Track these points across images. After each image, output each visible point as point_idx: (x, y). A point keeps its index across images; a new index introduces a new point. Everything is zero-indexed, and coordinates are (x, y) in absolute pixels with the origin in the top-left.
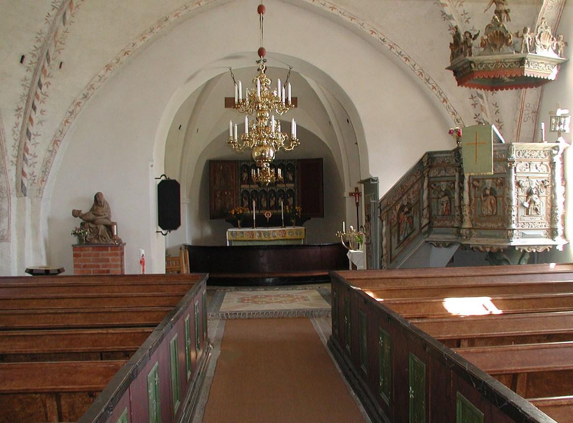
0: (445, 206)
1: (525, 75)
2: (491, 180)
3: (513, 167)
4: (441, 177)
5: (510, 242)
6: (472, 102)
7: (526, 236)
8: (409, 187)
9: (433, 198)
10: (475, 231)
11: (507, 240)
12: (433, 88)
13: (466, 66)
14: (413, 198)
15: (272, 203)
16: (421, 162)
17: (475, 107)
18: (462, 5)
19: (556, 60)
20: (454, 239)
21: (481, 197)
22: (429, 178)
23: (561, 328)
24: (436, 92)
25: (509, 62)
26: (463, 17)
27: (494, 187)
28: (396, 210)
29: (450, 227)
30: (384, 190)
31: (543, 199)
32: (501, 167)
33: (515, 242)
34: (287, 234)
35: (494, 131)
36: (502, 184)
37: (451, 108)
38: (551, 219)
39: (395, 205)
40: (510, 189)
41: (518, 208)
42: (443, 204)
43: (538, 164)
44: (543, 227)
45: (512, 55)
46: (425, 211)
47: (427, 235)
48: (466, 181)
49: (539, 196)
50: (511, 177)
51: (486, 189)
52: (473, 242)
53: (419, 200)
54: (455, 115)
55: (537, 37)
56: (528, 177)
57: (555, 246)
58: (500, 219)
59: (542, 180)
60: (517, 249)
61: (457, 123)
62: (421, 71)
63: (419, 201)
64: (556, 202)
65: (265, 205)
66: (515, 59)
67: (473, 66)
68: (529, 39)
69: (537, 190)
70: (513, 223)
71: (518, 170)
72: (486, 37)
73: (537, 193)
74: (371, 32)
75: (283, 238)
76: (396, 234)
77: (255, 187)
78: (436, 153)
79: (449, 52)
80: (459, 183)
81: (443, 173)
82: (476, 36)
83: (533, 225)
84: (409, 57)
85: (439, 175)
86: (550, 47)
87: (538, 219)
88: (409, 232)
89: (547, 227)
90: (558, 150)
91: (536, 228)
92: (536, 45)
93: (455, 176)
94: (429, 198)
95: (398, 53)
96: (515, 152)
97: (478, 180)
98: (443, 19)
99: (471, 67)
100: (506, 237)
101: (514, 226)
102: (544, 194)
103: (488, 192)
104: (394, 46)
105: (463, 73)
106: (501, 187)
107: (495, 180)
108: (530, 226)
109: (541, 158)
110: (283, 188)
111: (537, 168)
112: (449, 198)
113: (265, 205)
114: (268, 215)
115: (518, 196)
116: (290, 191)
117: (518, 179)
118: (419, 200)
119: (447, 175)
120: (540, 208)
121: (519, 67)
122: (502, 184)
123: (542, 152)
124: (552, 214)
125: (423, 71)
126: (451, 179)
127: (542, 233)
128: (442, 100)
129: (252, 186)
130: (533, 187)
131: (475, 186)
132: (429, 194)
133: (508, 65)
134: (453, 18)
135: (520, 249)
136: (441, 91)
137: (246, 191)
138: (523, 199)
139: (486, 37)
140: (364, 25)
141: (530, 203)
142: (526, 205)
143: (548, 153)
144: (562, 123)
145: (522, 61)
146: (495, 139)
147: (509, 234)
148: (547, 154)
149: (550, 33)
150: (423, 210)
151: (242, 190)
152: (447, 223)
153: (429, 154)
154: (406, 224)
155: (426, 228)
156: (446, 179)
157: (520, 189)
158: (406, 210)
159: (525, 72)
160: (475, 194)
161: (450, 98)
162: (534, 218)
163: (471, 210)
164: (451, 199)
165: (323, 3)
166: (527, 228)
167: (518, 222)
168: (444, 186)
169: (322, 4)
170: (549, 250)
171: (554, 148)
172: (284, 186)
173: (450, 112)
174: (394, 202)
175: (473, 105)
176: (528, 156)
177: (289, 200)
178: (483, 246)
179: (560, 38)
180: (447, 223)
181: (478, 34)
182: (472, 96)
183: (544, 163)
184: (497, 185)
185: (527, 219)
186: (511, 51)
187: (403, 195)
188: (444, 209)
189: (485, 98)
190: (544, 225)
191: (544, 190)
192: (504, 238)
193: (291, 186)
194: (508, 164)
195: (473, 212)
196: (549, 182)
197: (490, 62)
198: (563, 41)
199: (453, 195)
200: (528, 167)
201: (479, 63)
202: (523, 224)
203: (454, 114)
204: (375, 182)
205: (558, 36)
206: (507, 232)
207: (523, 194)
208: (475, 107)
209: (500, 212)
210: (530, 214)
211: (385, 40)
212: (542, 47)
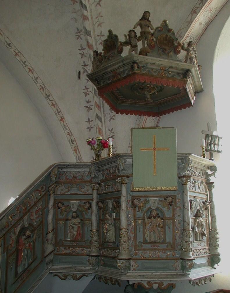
0: (76, 229)
4: (72, 195)
6: (88, 125)
8: (32, 204)
9: (61, 220)
10: (135, 263)
11: (181, 273)
14: (37, 218)
17: (90, 131)
18: (101, 26)
24: (55, 109)
25: (172, 72)
26: (98, 38)
28: (15, 233)
37: (68, 129)
39: (15, 226)
46: (50, 236)
53: (42, 222)
54: (70, 136)
61: (71, 144)
62: (43, 86)
63: (43, 223)
76: (14, 265)
80: (97, 203)
81: (74, 190)
84: (33, 69)
85: (69, 193)
88: (30, 261)
94: (56, 220)
95: (22, 62)
97: (138, 198)
104: (19, 54)
106: (171, 207)
118: (42, 222)
119: (79, 193)
125: (44, 85)
126: (89, 197)
128: (60, 118)
132: (55, 214)
134: (90, 34)
150: (47, 234)
152: (78, 250)
154: (28, 251)
155: (51, 257)
158: (28, 233)
161: (68, 119)
168: (75, 205)
173: (66, 132)
174: (13, 223)
175: (88, 128)
178: (149, 283)
182: (89, 119)
187: (25, 214)
189: (103, 122)
203: (69, 134)
208: (90, 131)
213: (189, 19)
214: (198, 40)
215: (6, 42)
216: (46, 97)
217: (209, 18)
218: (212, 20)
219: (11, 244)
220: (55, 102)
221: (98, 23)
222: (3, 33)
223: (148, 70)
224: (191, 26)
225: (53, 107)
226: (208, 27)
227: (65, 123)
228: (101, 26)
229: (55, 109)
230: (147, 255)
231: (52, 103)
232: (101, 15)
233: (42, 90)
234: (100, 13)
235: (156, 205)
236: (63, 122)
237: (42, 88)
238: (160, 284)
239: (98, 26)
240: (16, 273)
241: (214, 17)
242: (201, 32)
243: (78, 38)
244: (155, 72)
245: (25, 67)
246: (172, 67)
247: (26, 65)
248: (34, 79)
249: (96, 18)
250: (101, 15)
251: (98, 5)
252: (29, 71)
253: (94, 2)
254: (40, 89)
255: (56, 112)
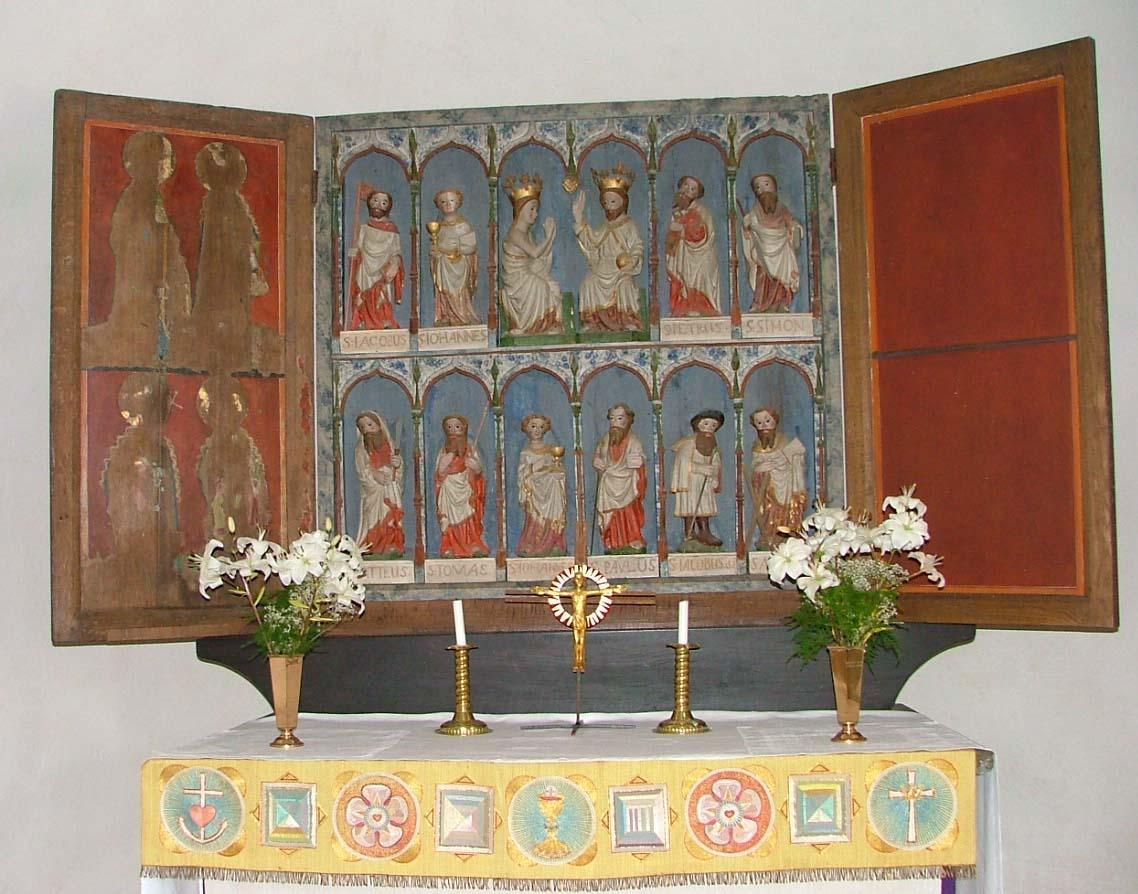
23: (319, 479)
53: (320, 822)
110: (716, 348)
114: (579, 603)
116: (776, 374)
129: (437, 340)
137: (375, 378)
151: (347, 375)
172: (718, 330)
177: (766, 460)
193: (790, 329)
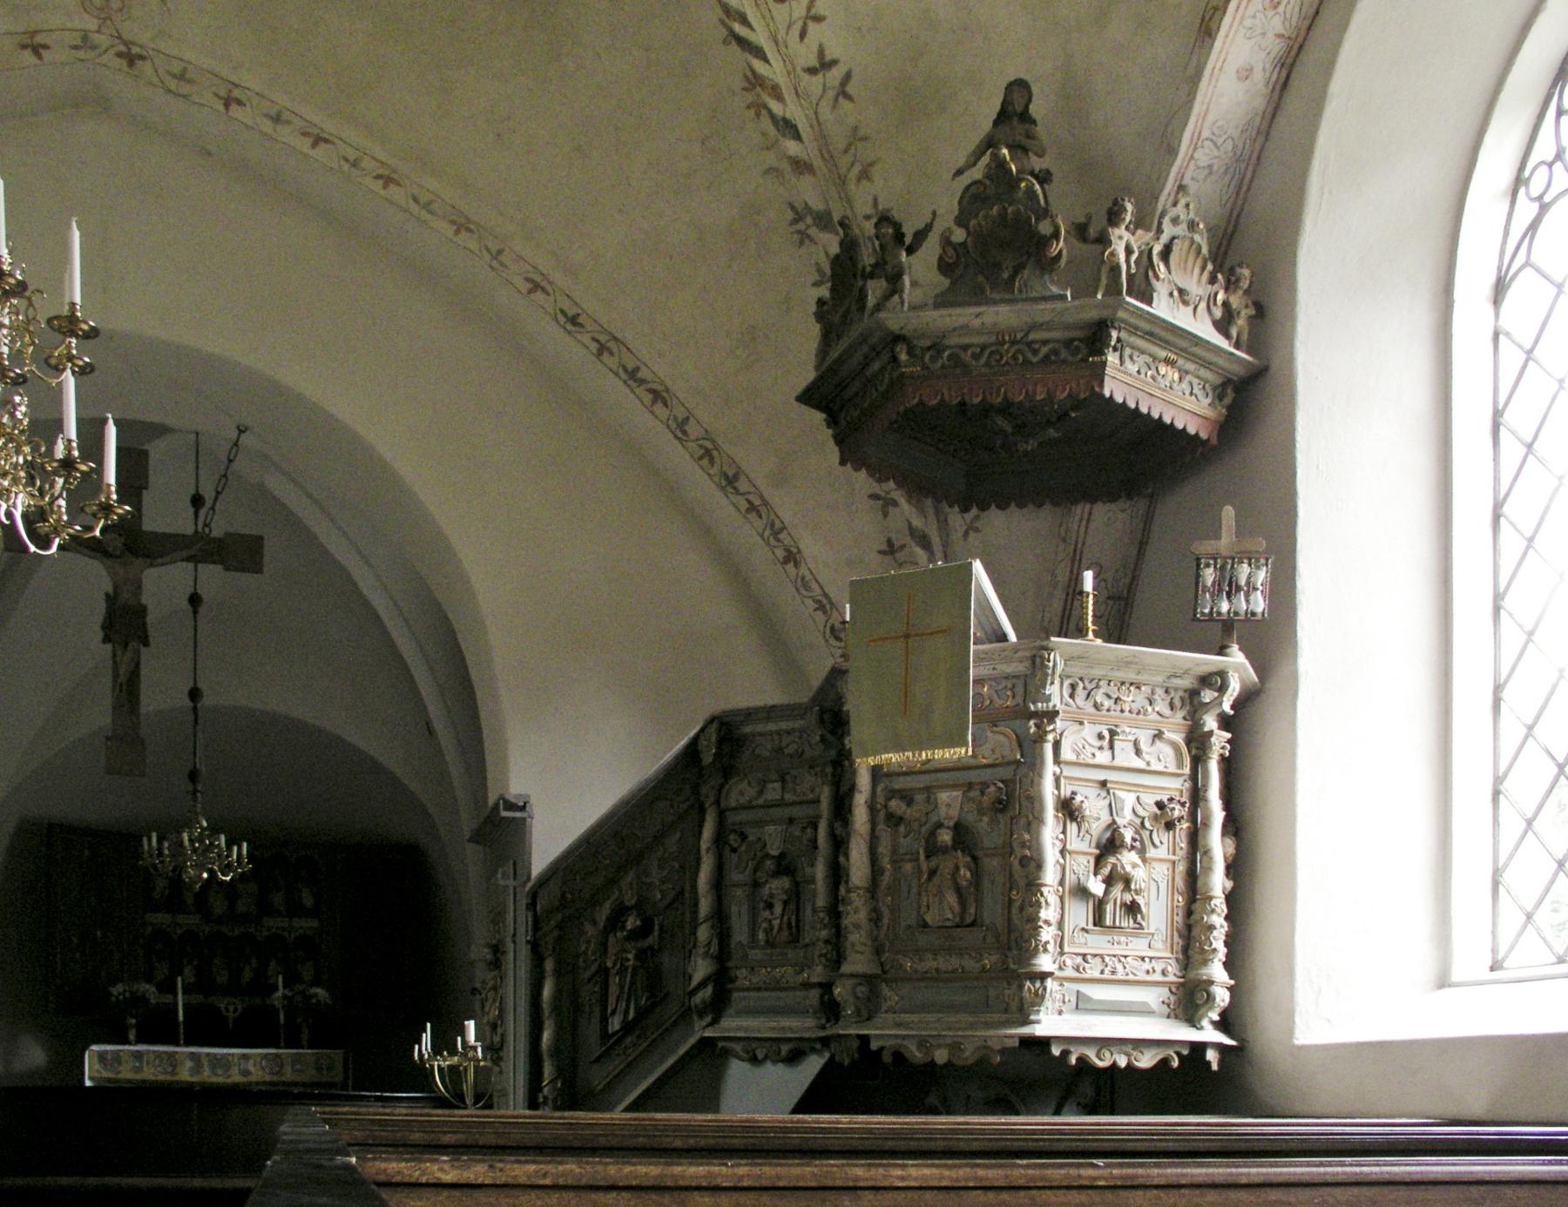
0: (778, 909)
1: (1107, 394)
2: (958, 793)
3: (1050, 737)
5: (1026, 1022)
7: (1089, 1006)
12: (748, 510)
13: (876, 366)
15: (247, 975)
16: (691, 753)
18: (869, 178)
19: (1227, 365)
20: (808, 1029)
21: (917, 860)
22: (721, 814)
24: (759, 524)
25: (1045, 342)
27: (971, 818)
28: (595, 923)
29: (794, 988)
30: (546, 845)
31: (1161, 872)
32: (1002, 738)
33: (1047, 1023)
34: (288, 1070)
35: (979, 586)
36: (1002, 806)
38: (1186, 950)
39: (594, 902)
40: (1034, 820)
41: (1061, 898)
42: (770, 906)
43: (1144, 738)
44: (1158, 977)
45: (1059, 305)
46: (703, 933)
47: (708, 1019)
48: (860, 800)
49: (1144, 860)
50: (1040, 776)
51: (940, 825)
52: (883, 1032)
53: (682, 892)
55: (1157, 249)
56: (1104, 784)
57: (1198, 1048)
58: (990, 939)
59: (1158, 798)
60: (1056, 1051)
62: (708, 445)
63: (684, 897)
64: (1206, 884)
65: (222, 978)
66: (1068, 327)
67: (903, 357)
68: (1129, 251)
69: (1137, 832)
70: (1045, 950)
71: (1067, 754)
72: (959, 235)
73: (1137, 844)
74: (530, 286)
75: (275, 1079)
77: (189, 920)
78: (749, 714)
79: (815, 329)
81: (773, 792)
82: (921, 235)
83: (1119, 967)
84: (667, 390)
85: (760, 801)
86: (1203, 305)
87: (1138, 946)
89: (1171, 978)
90: (1222, 689)
91: (1131, 977)
92: (1154, 281)
93: (817, 801)
95: (626, 370)
96: (1057, 681)
97: (907, 797)
98: (796, 237)
99: (895, 359)
100: (1014, 1005)
101: (1045, 962)
102: (1162, 852)
103: (946, 837)
104: (612, 345)
105: (873, 401)
107: (975, 794)
108: (1107, 971)
109: (1155, 717)
110: (284, 929)
111: (1138, 752)
112: (797, 884)
113: (222, 978)
115: (1063, 852)
117: (1066, 791)
119: (789, 797)
120: (1147, 904)
121: (1085, 360)
122: (1002, 806)
123: (1160, 692)
124: (1189, 928)
125: (713, 441)
127: (1154, 997)
128: (780, 553)
130: (1120, 821)
131: (894, 820)
133: (1041, 355)
135: (1066, 1053)
136: (778, 525)
138: (1081, 866)
139: (959, 235)
140: (503, 258)
141: (1109, 881)
142: (1097, 887)
143: (1182, 699)
144: (1243, 582)
145: (1095, 338)
146: (982, 618)
147: (1026, 994)
148: (1177, 703)
149: (1205, 250)
152: (786, 973)
153: (722, 724)
156: (787, 812)
157: (1074, 825)
158: (632, 922)
159: (1107, 379)
160: (894, 851)
161: (810, 547)
162: (1123, 939)
163: (875, 910)
164: (796, 896)
165: (352, 158)
166: (1097, 974)
167: (1062, 953)
169: (347, 160)
170: (1175, 1064)
171: (1205, 681)
176: (1107, 703)
178: (922, 1043)
179: (1238, 280)
180: (786, 973)
181: (929, 227)
182: (890, 542)
183: (1167, 735)
184: (981, 812)
185: (1098, 942)
186: (1055, 290)
188: (776, 923)
190: (1159, 966)
191: (1165, 840)
192: (1006, 1011)
194: (1032, 723)
195: (886, 921)
196: (1183, 805)
197: (966, 340)
198: (1247, 292)
199: (808, 870)
200: (1106, 743)
201: (928, 343)
202: (1079, 960)
204: (518, 814)
205: (1232, 270)
206: (1021, 987)
207: (1082, 844)
209: (992, 911)
210: (1108, 922)
211: (580, 320)
212: (1176, 293)
213: (1191, 71)
214: (1261, 139)
215: (562, 311)
216: (724, 483)
217: (1279, 36)
218: (1300, 40)
219: (585, 953)
220: (762, 497)
221: (857, 169)
222: (551, 283)
223: (950, 357)
224: (1199, 98)
225: (752, 516)
226: (1294, 75)
227: (803, 571)
228: (869, 178)
229: (759, 524)
230: (930, 964)
231: (749, 501)
232: (862, 132)
233: (705, 462)
234: (856, 128)
235: (954, 813)
236: (796, 565)
237: (708, 453)
238: (955, 1047)
239: (859, 180)
240: (605, 1035)
241: (1307, 23)
242: (1260, 103)
243: (802, 243)
244: (976, 357)
245: (637, 391)
246: (1034, 327)
247: (642, 381)
248: (674, 426)
249: (846, 151)
250: (862, 132)
251: (841, 99)
252: (654, 402)
253: (824, 91)
254: (701, 458)
255: (767, 533)
